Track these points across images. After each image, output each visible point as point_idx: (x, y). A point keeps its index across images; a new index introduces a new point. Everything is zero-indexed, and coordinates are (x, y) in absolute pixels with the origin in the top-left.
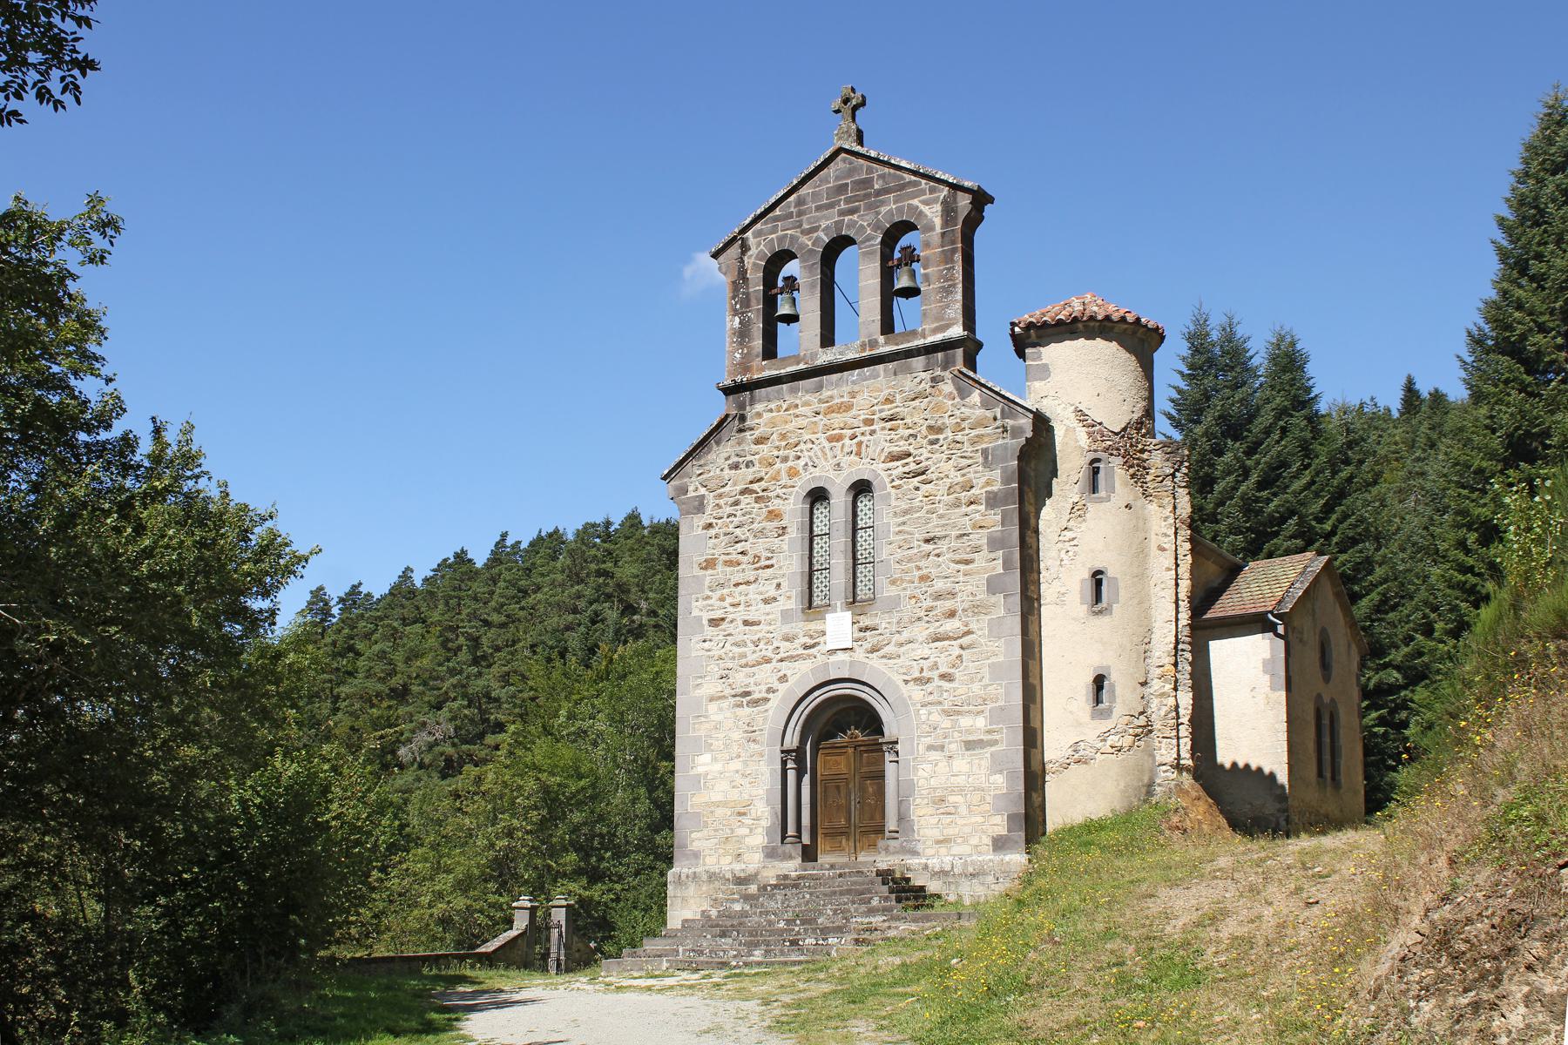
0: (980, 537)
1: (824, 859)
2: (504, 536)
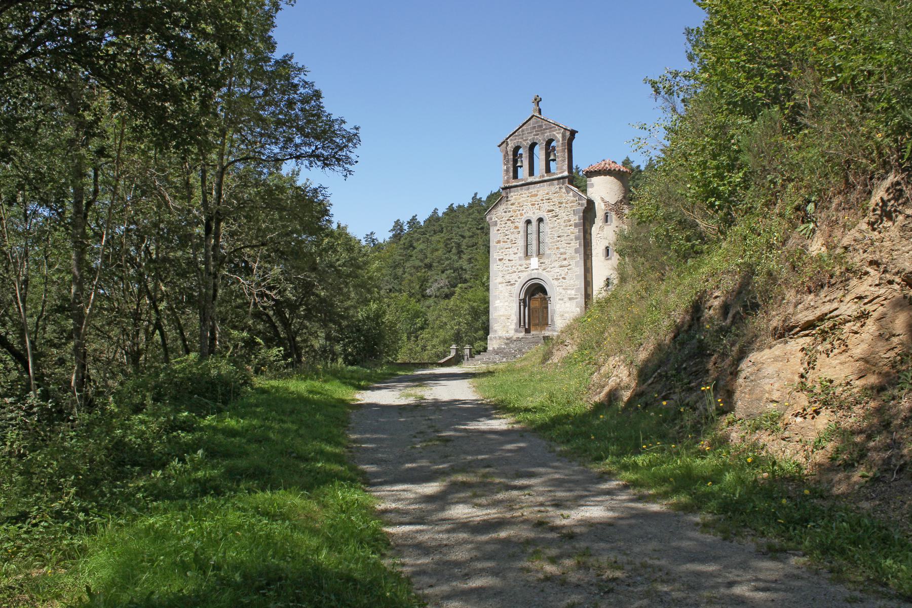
0: (573, 237)
1: (532, 333)
2: (476, 194)
